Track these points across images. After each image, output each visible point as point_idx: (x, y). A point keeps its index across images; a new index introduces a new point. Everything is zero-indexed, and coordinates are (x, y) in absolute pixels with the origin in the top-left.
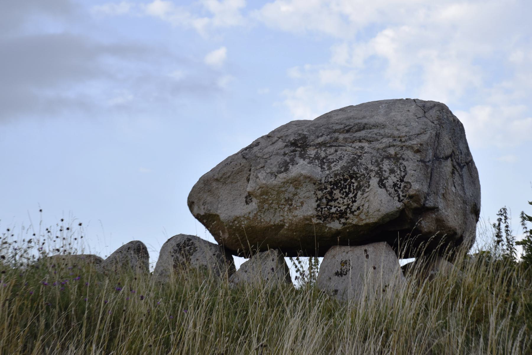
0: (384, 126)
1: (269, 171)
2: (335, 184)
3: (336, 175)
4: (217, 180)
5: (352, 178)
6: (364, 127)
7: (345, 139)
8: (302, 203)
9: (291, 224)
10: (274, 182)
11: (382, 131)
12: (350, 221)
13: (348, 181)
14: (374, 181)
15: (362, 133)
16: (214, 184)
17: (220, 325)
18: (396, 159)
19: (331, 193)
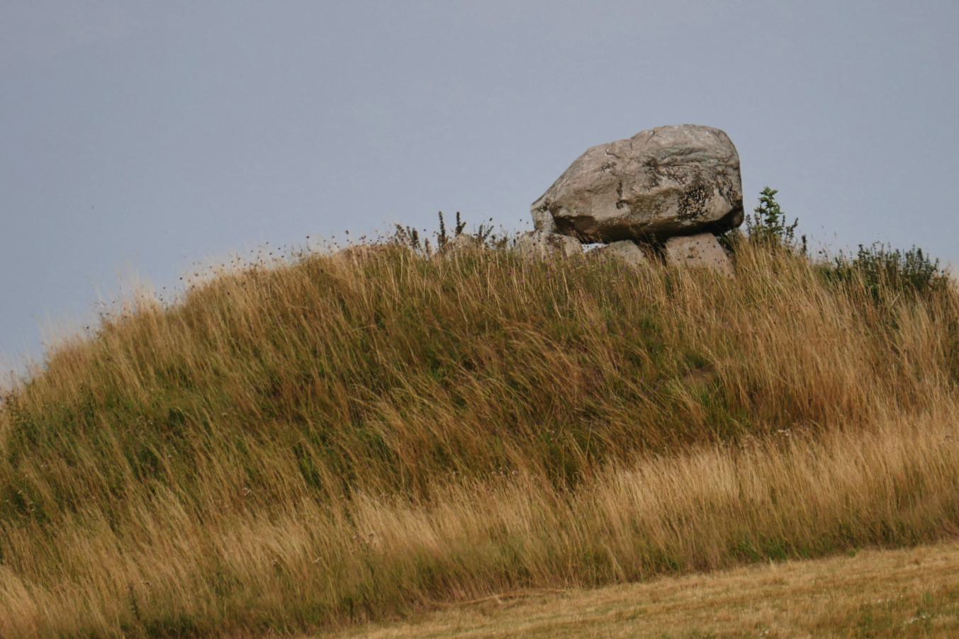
0: (705, 150)
1: (641, 185)
2: (689, 194)
3: (690, 187)
4: (589, 191)
5: (700, 189)
6: (692, 151)
7: (682, 160)
8: (668, 208)
9: (655, 223)
10: (648, 193)
11: (706, 154)
12: (698, 220)
13: (698, 191)
14: (716, 191)
15: (693, 156)
16: (587, 194)
17: (141, 475)
18: (724, 174)
19: (687, 200)
